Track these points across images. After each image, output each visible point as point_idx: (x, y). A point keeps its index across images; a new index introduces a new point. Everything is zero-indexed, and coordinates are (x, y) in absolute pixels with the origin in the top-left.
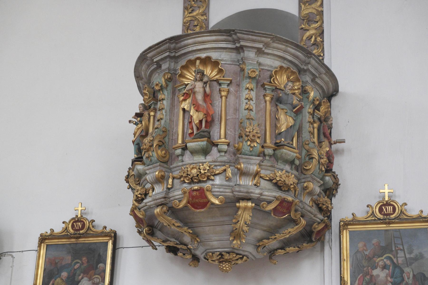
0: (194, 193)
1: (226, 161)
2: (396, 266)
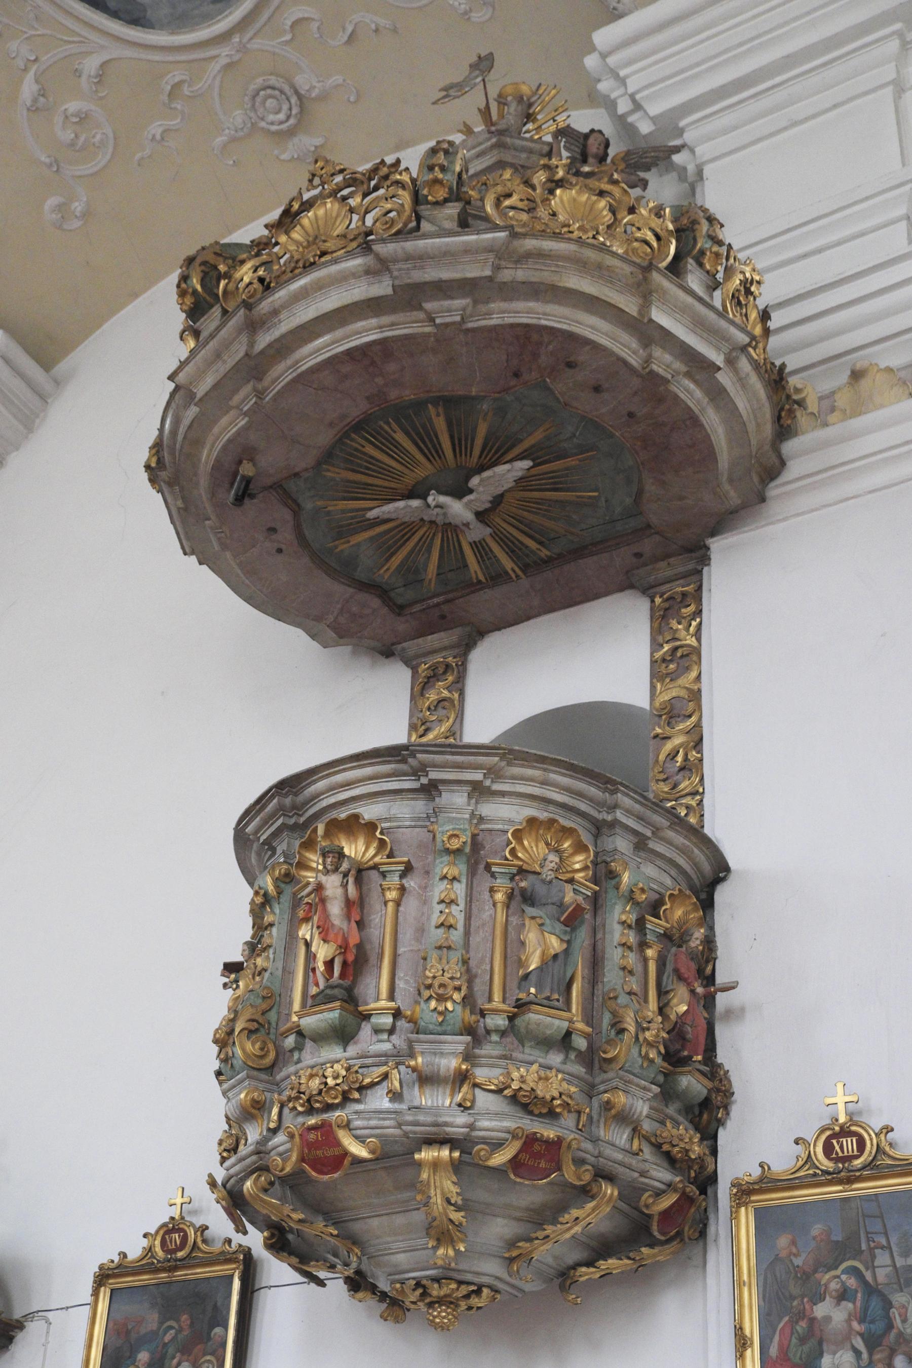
0: (312, 1136)
1: (389, 1053)
2: (871, 1290)
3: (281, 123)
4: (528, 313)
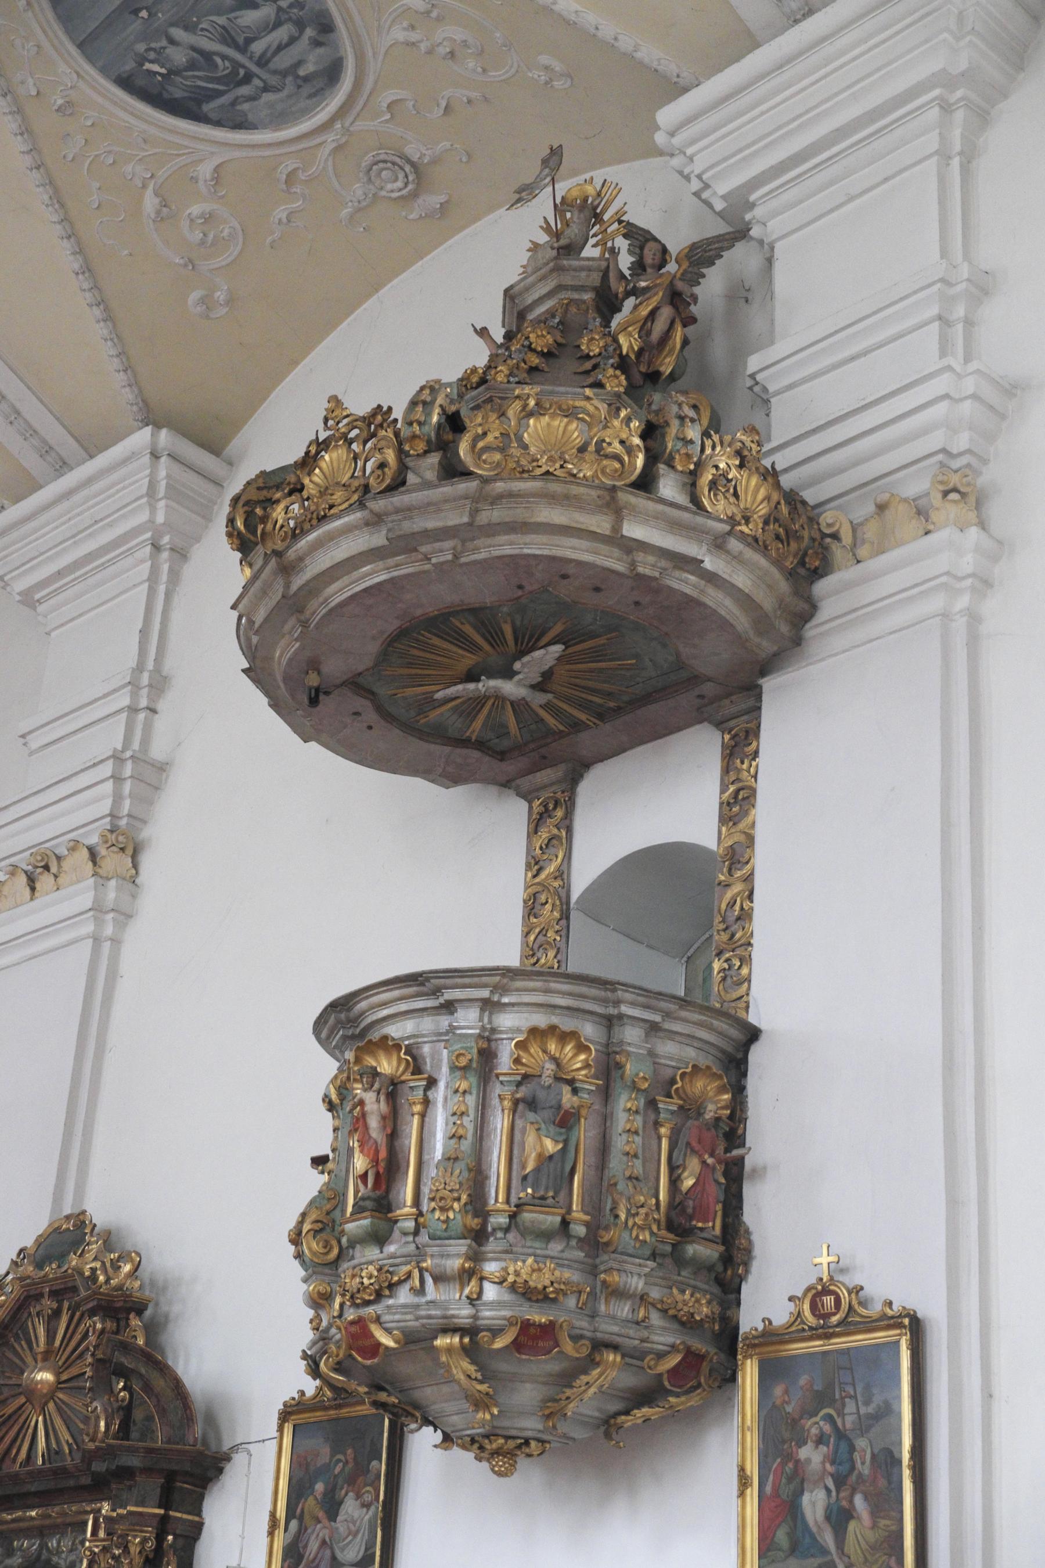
2: (841, 1435)
3: (400, 190)
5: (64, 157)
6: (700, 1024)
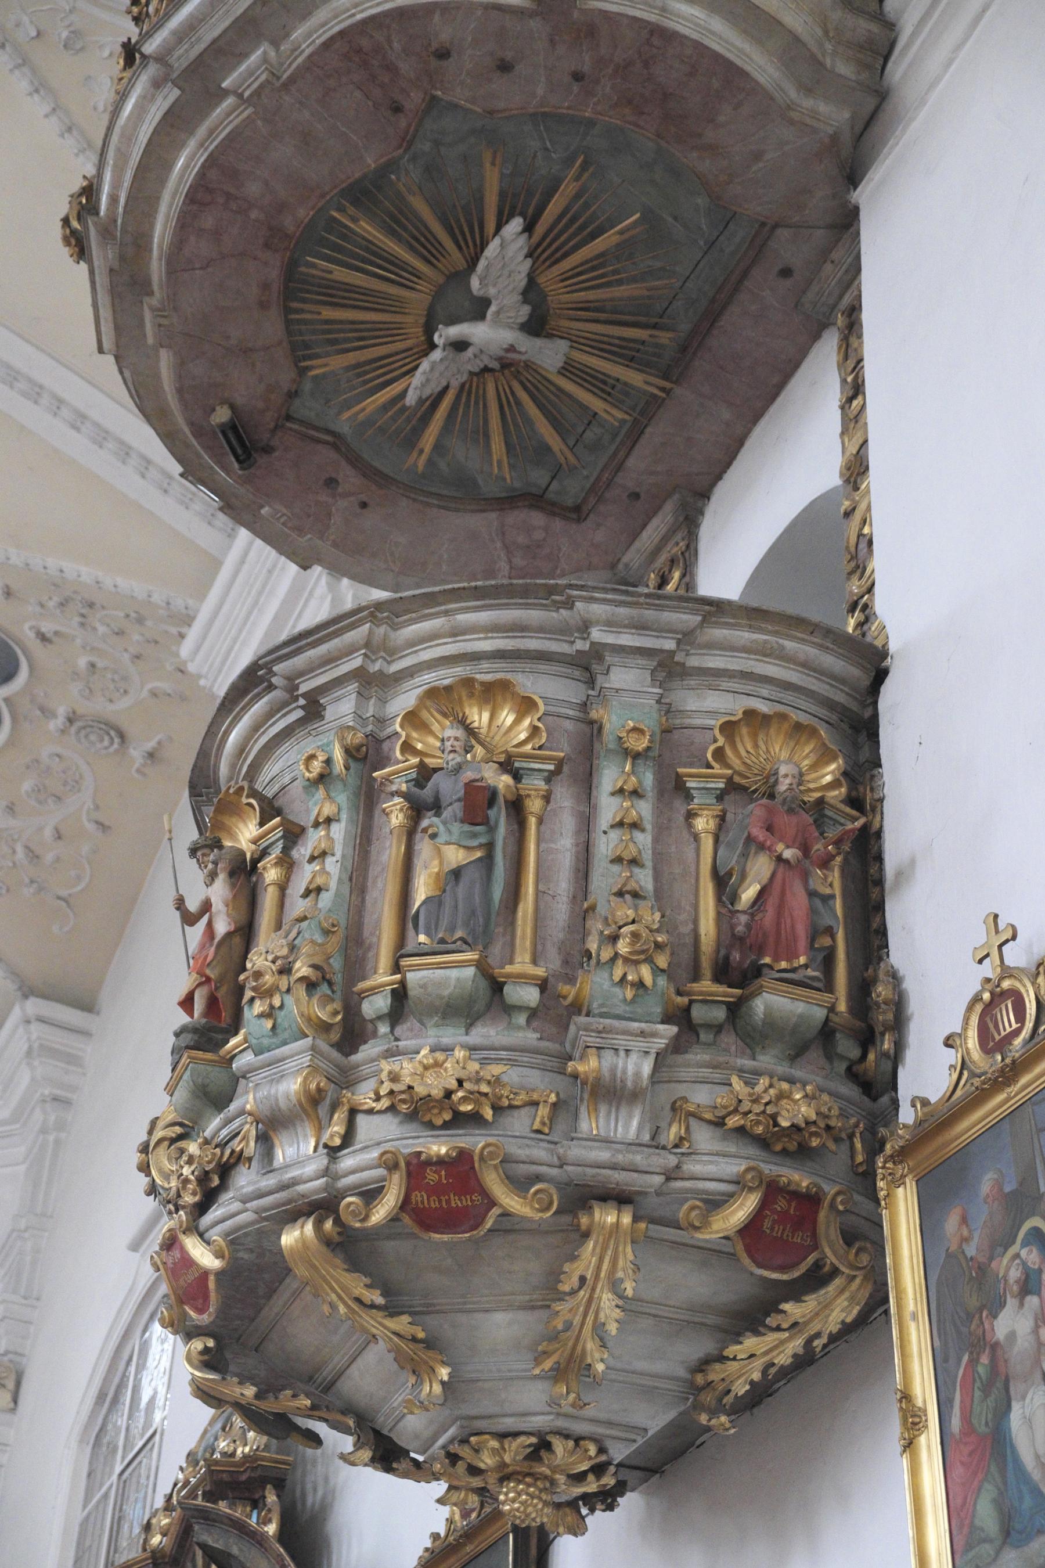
4: (336, 17)
5: (95, 109)
6: (764, 652)
